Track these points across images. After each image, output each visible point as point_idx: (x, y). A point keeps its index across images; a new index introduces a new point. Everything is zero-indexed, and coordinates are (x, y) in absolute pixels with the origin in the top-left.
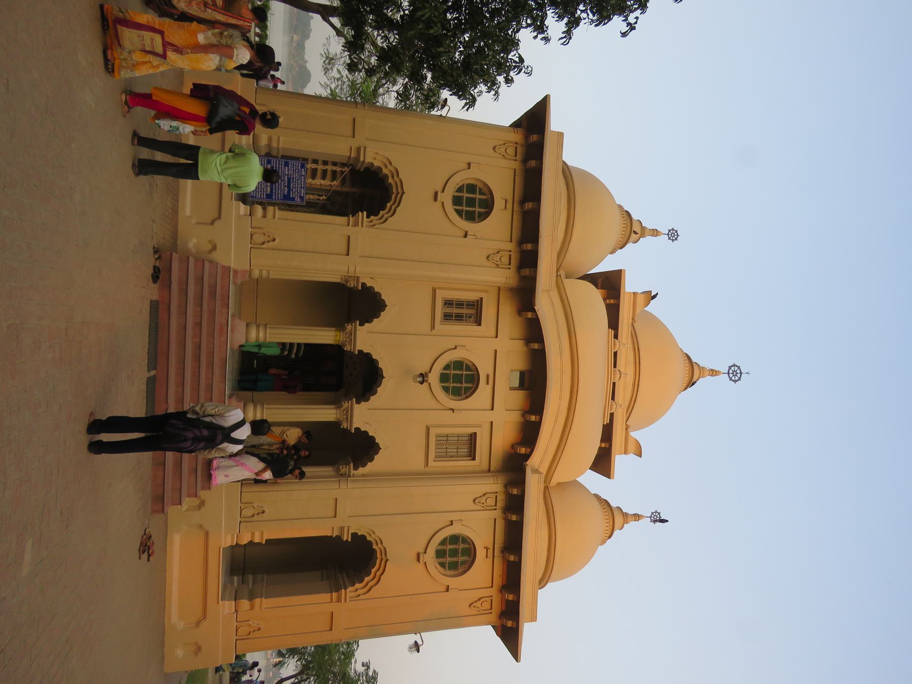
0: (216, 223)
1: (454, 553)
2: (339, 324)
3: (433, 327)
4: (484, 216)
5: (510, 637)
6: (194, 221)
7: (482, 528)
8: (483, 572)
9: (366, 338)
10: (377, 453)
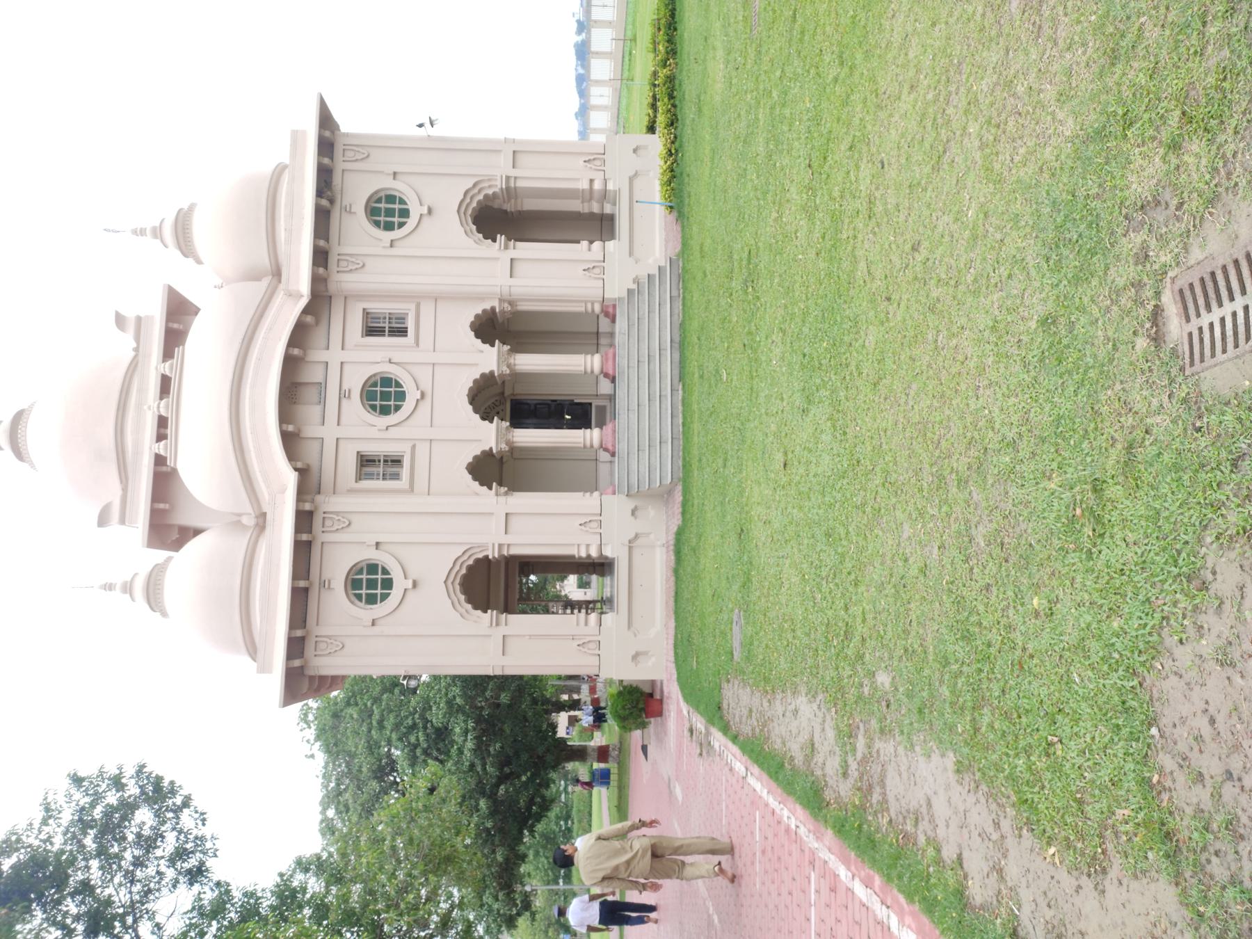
0: (633, 535)
1: (390, 213)
2: (514, 450)
3: (414, 447)
4: (356, 569)
5: (326, 120)
6: (652, 536)
7: (357, 233)
8: (357, 190)
9: (488, 435)
10: (469, 464)
